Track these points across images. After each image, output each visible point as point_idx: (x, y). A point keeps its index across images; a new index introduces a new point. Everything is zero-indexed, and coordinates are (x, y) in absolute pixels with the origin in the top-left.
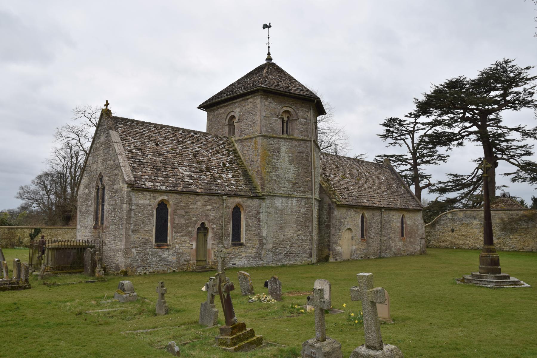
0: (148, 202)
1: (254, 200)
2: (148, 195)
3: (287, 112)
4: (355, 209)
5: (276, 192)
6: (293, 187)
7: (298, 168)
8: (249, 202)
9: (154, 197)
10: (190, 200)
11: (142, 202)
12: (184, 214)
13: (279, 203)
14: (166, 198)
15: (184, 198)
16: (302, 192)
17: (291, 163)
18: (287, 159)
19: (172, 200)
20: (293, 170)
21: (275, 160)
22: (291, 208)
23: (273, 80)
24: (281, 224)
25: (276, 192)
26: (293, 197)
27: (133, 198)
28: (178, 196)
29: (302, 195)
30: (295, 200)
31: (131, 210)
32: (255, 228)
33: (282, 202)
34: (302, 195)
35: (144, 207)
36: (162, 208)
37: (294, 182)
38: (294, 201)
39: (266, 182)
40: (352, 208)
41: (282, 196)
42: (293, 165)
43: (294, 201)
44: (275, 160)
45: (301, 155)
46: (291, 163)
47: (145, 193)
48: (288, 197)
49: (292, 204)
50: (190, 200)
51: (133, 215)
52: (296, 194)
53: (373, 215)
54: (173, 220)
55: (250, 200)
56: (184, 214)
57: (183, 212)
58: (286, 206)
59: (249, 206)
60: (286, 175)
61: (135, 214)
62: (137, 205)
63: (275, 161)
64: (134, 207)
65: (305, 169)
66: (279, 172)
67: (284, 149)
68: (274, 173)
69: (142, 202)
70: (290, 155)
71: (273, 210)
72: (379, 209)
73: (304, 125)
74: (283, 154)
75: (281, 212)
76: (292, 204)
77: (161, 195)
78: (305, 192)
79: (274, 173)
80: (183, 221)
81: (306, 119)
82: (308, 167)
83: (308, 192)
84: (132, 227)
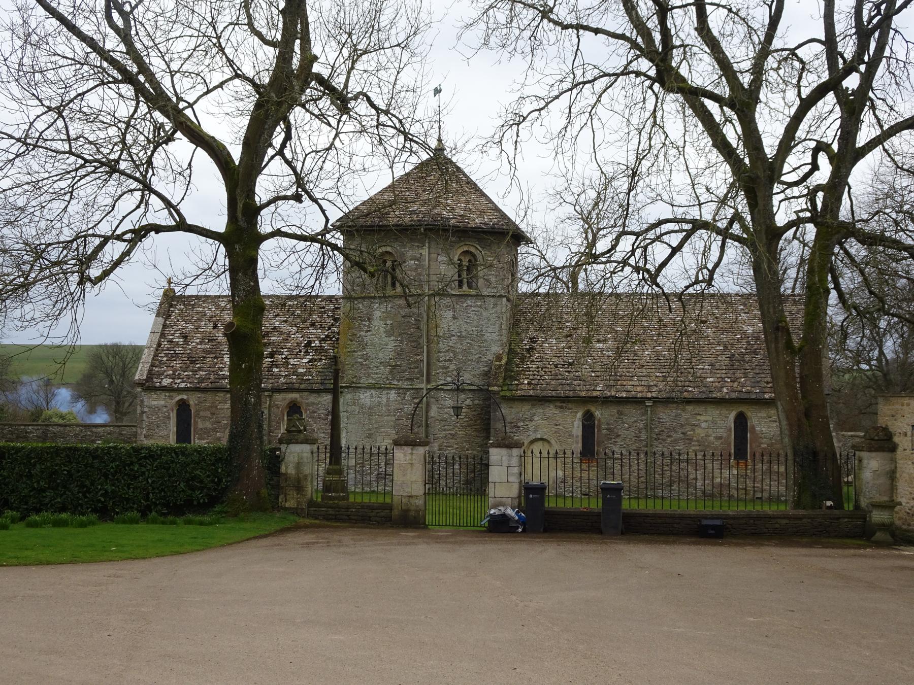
0: (163, 403)
1: (323, 395)
2: (163, 395)
3: (466, 253)
4: (559, 404)
5: (362, 381)
6: (391, 372)
7: (401, 341)
8: (312, 398)
9: (171, 397)
10: (217, 398)
11: (155, 403)
12: (210, 416)
13: (366, 397)
14: (185, 397)
15: (209, 396)
16: (407, 379)
17: (389, 334)
18: (382, 330)
19: (193, 400)
20: (391, 345)
21: (362, 333)
22: (388, 405)
23: (453, 210)
24: (370, 430)
25: (362, 381)
26: (390, 389)
27: (145, 399)
28: (200, 395)
29: (406, 384)
30: (393, 392)
31: (143, 412)
32: (323, 435)
33: (372, 396)
34: (406, 384)
35: (159, 408)
36: (183, 409)
37: (394, 363)
38: (393, 394)
39: (346, 367)
40: (550, 401)
41: (370, 387)
42: (392, 338)
43: (393, 394)
44: (362, 333)
45: (408, 319)
46: (389, 334)
47: (158, 392)
48: (380, 388)
49: (388, 399)
50: (217, 398)
51: (145, 418)
52: (396, 383)
53: (620, 413)
54: (196, 422)
55: (314, 395)
56: (210, 416)
57: (208, 414)
58: (379, 402)
59: (314, 404)
60: (381, 355)
61: (148, 417)
62: (150, 407)
63: (362, 333)
64: (146, 410)
65: (413, 341)
66: (369, 350)
67: (377, 314)
68: (360, 353)
69: (155, 403)
70: (389, 322)
71: (357, 409)
72: (636, 401)
73: (416, 270)
74: (377, 323)
75: (370, 412)
76: (388, 399)
77: (179, 394)
78: (412, 380)
79: (360, 353)
80: (208, 425)
81: (419, 260)
82: (420, 337)
83: (417, 379)
84: (144, 432)
